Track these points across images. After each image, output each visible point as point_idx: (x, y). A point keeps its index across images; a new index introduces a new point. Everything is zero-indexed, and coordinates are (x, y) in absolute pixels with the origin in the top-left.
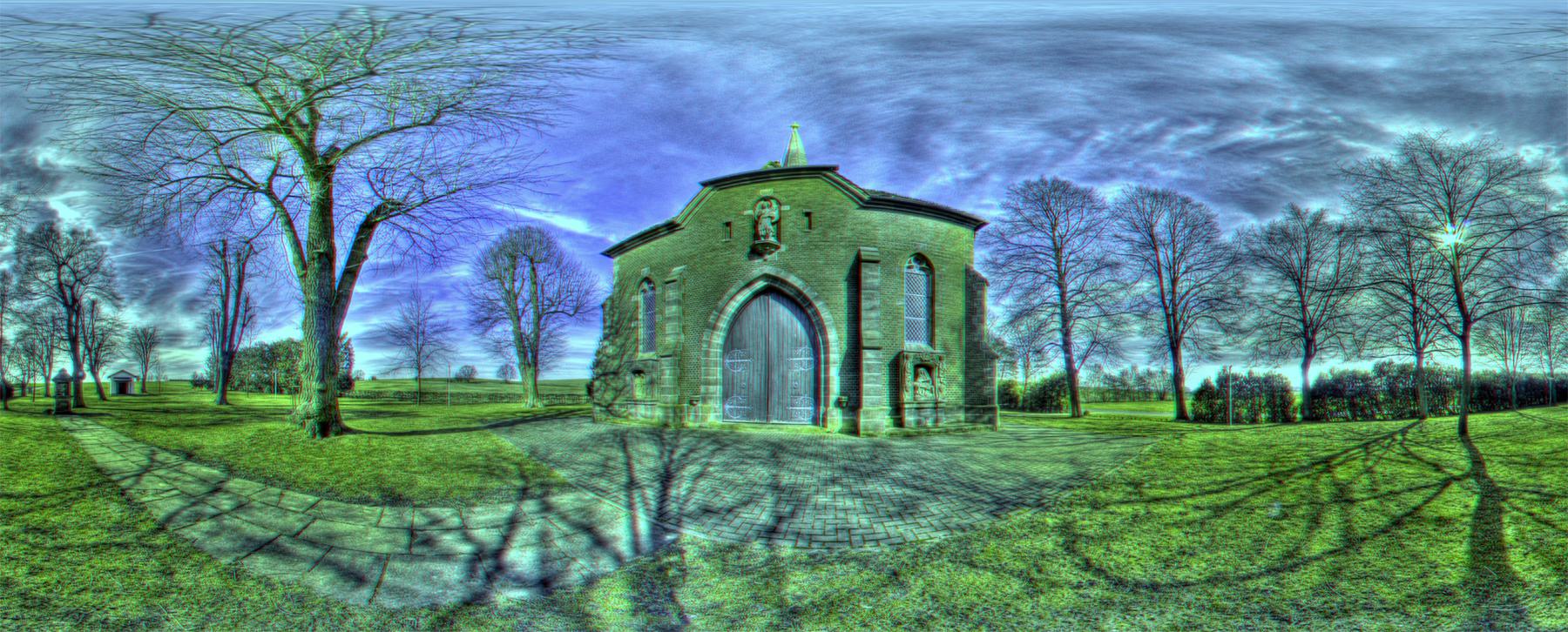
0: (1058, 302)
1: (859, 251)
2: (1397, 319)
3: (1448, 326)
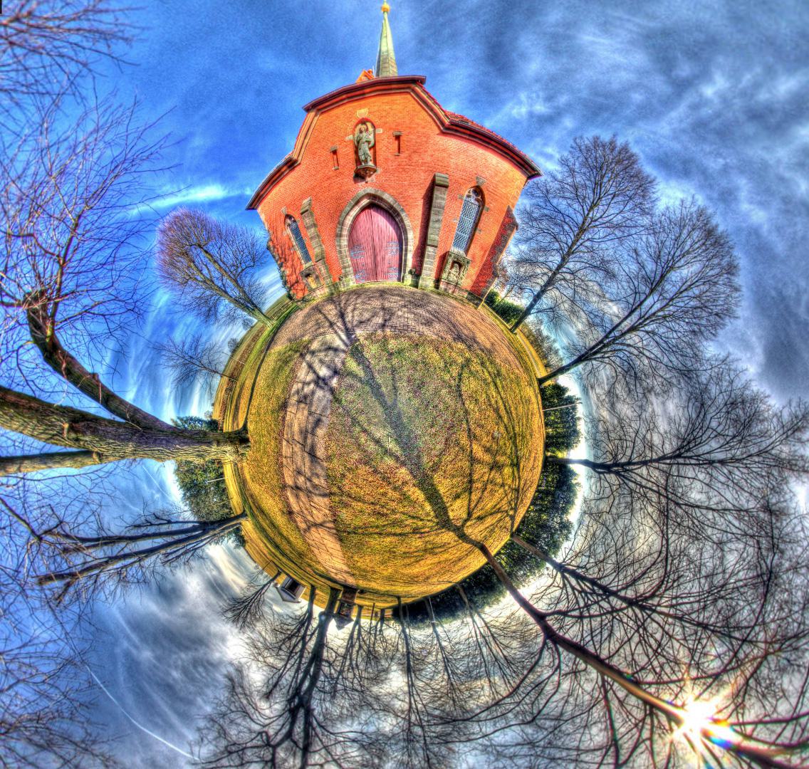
0: (554, 269)
1: (435, 176)
2: (609, 567)
3: (565, 614)
